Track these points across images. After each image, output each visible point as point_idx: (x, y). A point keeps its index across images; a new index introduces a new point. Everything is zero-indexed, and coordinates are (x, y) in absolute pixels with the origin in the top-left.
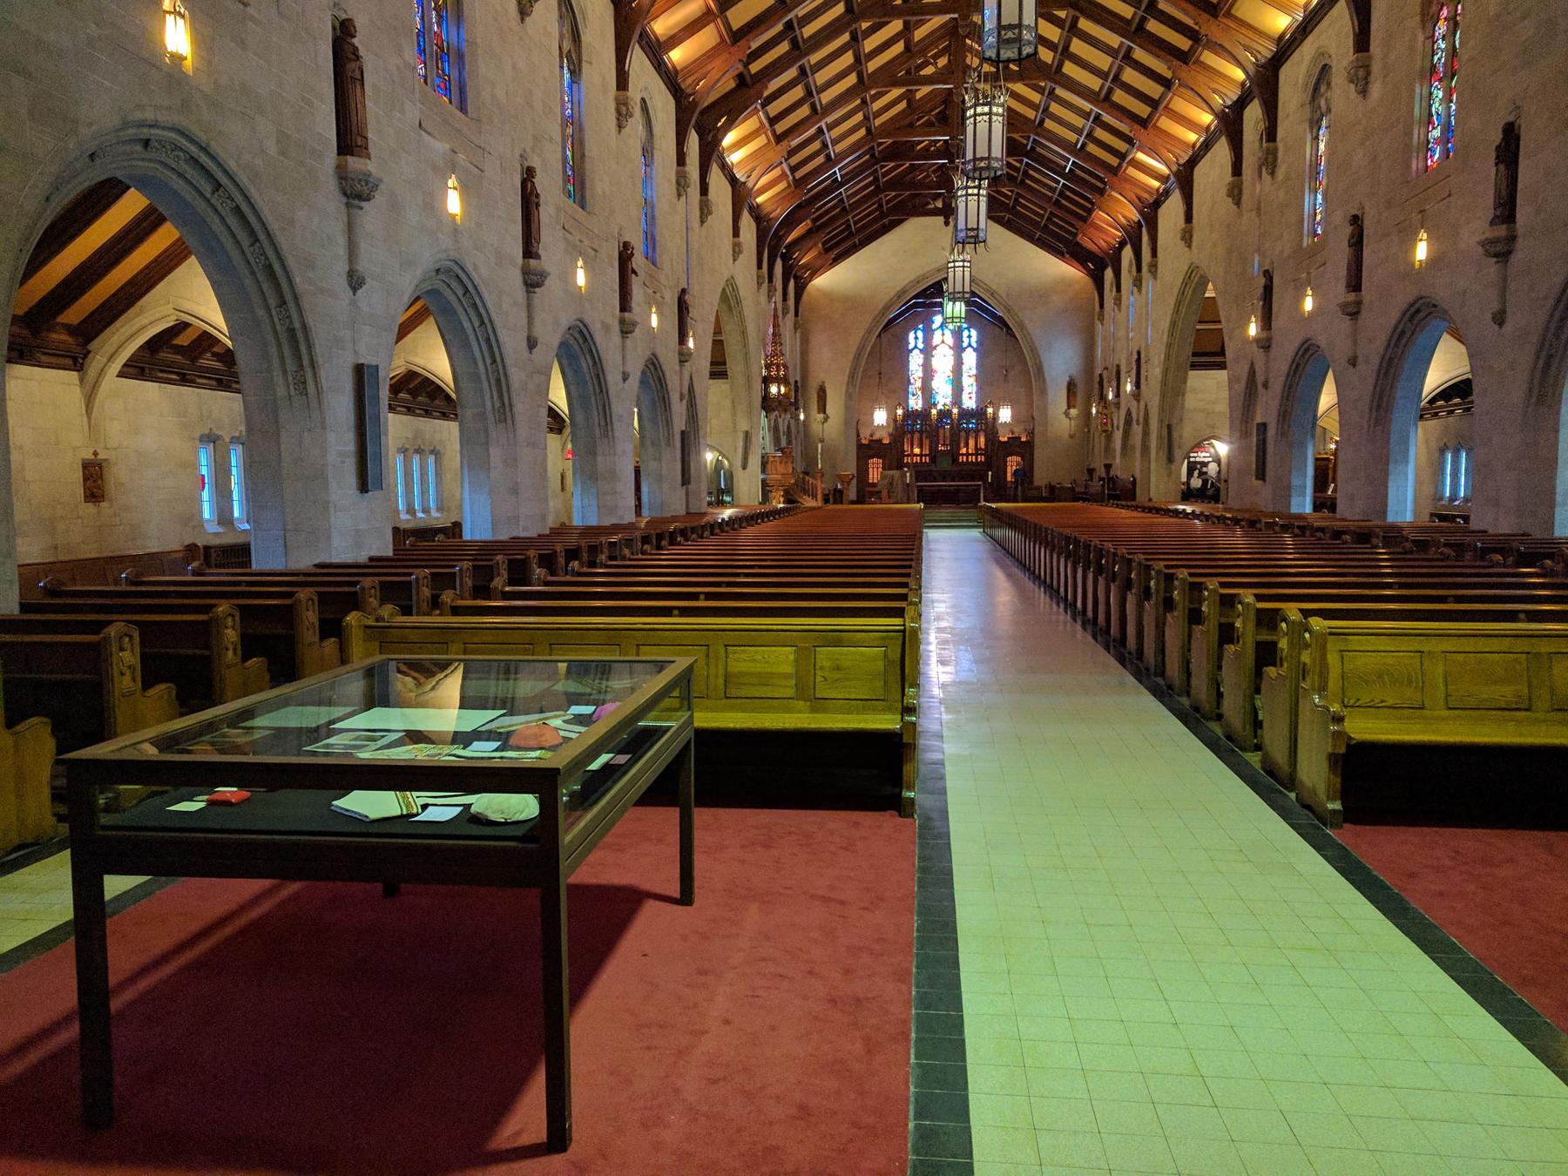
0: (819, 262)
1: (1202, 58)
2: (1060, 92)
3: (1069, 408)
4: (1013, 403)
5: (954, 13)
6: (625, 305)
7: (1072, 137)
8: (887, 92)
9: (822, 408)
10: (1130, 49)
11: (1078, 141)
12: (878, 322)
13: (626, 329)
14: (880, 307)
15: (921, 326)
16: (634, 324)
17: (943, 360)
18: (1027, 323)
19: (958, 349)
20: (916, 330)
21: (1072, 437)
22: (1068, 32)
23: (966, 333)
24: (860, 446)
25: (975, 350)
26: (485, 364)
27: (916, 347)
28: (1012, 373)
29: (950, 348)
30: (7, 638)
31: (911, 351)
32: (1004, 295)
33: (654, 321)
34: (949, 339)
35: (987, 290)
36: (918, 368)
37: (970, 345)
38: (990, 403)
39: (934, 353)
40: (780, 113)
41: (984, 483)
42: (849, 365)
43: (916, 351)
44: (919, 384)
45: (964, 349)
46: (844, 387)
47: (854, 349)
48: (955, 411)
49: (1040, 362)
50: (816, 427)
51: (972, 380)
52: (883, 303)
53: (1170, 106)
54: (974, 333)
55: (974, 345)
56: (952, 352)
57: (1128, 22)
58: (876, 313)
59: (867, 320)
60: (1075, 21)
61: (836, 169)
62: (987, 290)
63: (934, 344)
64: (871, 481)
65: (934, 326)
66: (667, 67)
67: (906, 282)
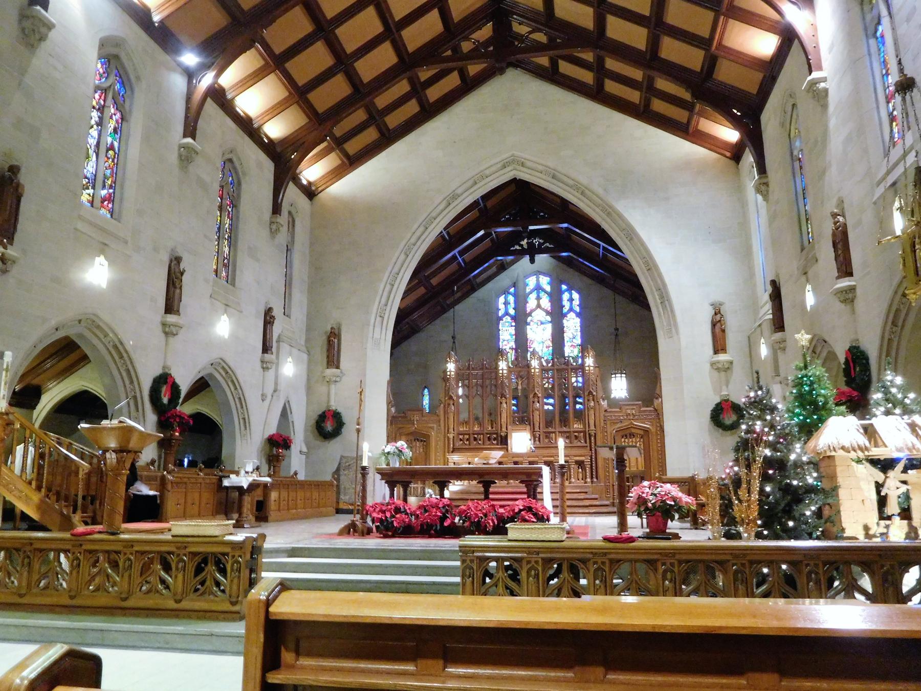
2: (611, 64)
5: (596, 494)
6: (171, 307)
19: (557, 315)
23: (566, 296)
25: (578, 315)
26: (222, 376)
29: (548, 313)
31: (501, 319)
34: (546, 302)
36: (509, 337)
37: (571, 309)
39: (529, 319)
45: (565, 315)
54: (576, 296)
55: (577, 309)
56: (549, 318)
60: (600, 61)
61: (456, 251)
63: (528, 310)
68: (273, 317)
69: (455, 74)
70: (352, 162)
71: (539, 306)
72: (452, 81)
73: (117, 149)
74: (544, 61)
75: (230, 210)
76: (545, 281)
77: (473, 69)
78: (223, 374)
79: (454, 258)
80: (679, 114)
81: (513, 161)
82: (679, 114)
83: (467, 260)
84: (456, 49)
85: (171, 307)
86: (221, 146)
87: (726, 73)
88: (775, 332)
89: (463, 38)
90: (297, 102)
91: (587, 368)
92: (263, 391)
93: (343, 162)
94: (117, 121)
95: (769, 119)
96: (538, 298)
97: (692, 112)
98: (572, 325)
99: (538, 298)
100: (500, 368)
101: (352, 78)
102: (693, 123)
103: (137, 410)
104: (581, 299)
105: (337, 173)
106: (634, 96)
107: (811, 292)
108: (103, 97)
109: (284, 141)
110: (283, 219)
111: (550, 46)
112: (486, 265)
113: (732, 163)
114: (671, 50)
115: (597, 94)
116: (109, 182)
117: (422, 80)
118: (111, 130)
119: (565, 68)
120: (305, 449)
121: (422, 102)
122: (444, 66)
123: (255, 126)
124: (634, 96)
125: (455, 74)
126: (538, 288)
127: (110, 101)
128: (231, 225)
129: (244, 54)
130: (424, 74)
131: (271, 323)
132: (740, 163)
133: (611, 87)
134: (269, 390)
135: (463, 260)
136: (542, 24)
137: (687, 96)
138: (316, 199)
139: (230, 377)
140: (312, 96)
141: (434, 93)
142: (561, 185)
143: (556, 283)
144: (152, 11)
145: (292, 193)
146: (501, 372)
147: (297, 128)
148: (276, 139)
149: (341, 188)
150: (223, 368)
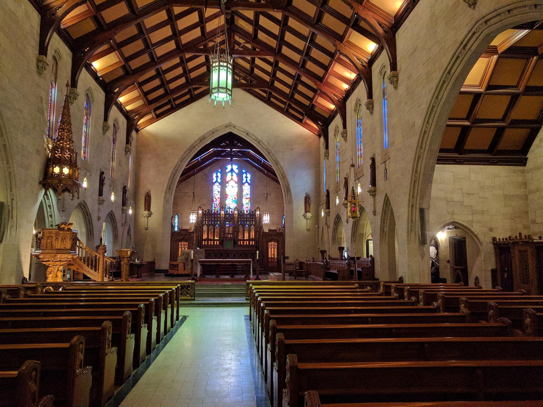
3: (306, 212)
4: (271, 214)
6: (101, 194)
7: (283, 106)
8: (199, 88)
9: (148, 207)
10: (299, 76)
11: (285, 107)
13: (101, 202)
14: (188, 146)
15: (220, 170)
16: (103, 201)
17: (232, 190)
18: (279, 160)
19: (240, 183)
23: (244, 175)
24: (173, 233)
25: (249, 184)
27: (217, 181)
28: (269, 198)
29: (236, 182)
30: (2, 311)
32: (266, 143)
33: (113, 198)
34: (235, 178)
35: (256, 140)
37: (247, 182)
39: (227, 185)
41: (253, 260)
42: (167, 180)
43: (217, 184)
44: (218, 202)
45: (244, 184)
46: (163, 194)
49: (289, 185)
50: (143, 220)
51: (248, 201)
52: (192, 142)
54: (249, 175)
55: (249, 181)
56: (236, 185)
57: (288, 95)
58: (185, 149)
59: (180, 153)
60: (277, 63)
61: (199, 157)
62: (256, 140)
63: (227, 180)
64: (270, 256)
65: (227, 171)
66: (118, 103)
67: (206, 132)
68: (126, 190)
69: (196, 13)
70: (159, 117)
71: (232, 179)
76: (235, 167)
79: (198, 159)
80: (301, 117)
82: (301, 117)
88: (327, 209)
89: (210, 40)
90: (142, 99)
93: (140, 95)
96: (232, 175)
97: (316, 94)
99: (232, 175)
104: (251, 178)
105: (151, 122)
109: (132, 111)
111: (252, 52)
113: (318, 137)
125: (196, 13)
126: (232, 171)
130: (188, 56)
136: (248, 74)
138: (139, 132)
140: (148, 96)
143: (239, 169)
145: (114, 110)
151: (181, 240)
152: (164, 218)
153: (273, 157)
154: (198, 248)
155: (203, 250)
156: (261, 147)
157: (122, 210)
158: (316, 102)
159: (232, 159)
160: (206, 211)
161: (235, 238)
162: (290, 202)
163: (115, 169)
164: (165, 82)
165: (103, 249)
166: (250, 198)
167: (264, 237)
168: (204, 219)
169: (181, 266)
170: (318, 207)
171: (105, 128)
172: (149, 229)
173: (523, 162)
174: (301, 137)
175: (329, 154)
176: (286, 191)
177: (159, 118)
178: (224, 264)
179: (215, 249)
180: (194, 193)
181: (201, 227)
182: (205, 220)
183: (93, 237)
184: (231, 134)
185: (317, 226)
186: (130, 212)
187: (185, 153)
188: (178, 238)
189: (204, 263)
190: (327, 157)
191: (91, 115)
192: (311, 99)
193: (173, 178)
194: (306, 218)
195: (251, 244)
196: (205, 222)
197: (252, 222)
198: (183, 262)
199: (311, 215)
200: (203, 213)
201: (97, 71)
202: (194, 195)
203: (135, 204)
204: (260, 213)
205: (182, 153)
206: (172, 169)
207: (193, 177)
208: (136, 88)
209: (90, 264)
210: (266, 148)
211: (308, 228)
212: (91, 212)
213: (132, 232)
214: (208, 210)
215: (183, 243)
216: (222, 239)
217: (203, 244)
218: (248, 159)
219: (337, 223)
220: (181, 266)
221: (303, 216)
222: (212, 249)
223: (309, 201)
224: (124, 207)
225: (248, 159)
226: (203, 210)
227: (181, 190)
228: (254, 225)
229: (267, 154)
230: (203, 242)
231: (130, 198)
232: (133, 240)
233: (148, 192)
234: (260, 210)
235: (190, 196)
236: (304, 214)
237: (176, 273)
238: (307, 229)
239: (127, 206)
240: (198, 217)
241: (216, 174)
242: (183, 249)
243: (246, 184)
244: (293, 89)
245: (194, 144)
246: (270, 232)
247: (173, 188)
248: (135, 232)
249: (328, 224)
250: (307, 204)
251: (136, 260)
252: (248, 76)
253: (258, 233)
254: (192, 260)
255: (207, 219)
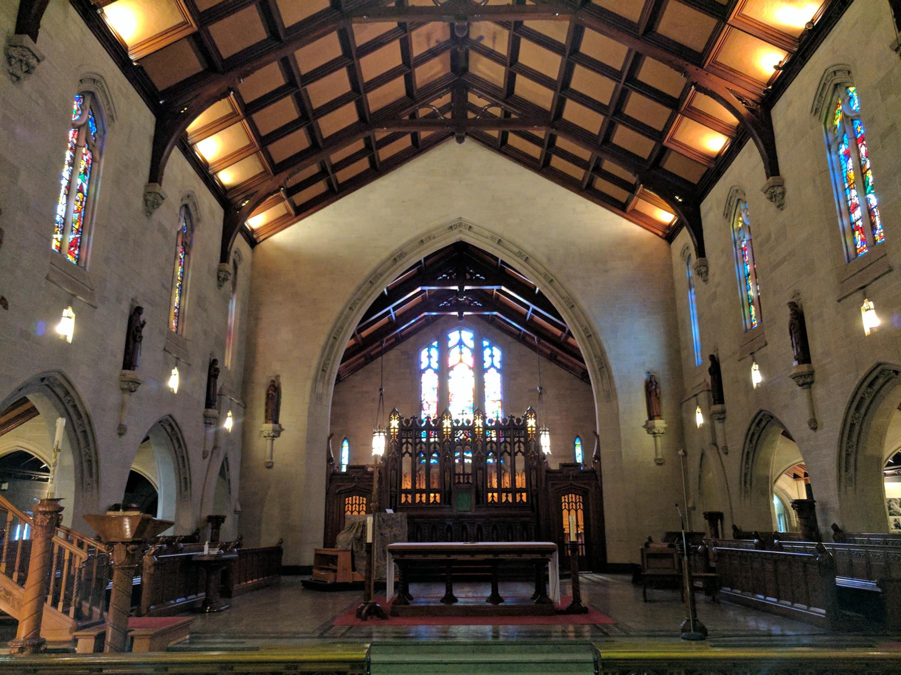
0: (263, 189)
1: (637, 208)
2: (562, 142)
3: (651, 417)
6: (129, 362)
9: (273, 414)
12: (365, 293)
14: (367, 272)
15: (435, 344)
19: (479, 370)
20: (430, 346)
21: (659, 463)
22: (547, 149)
23: (487, 352)
24: (333, 476)
25: (498, 371)
27: (429, 367)
29: (470, 368)
31: (423, 371)
32: (544, 260)
34: (469, 359)
35: (520, 254)
38: (531, 411)
40: (304, 181)
42: (318, 352)
45: (486, 371)
46: (309, 384)
47: (327, 328)
48: (479, 422)
49: (603, 353)
50: (261, 445)
52: (374, 265)
53: (693, 105)
54: (497, 352)
55: (498, 366)
56: (471, 373)
58: (359, 281)
59: (348, 290)
60: (552, 139)
61: (390, 308)
62: (520, 254)
63: (450, 365)
65: (450, 344)
66: (198, 159)
67: (404, 240)
68: (217, 370)
70: (301, 211)
72: (405, 142)
73: (85, 191)
74: (495, 133)
75: (182, 257)
77: (424, 134)
78: (169, 430)
79: (389, 312)
81: (460, 225)
82: (620, 194)
83: (397, 315)
84: (413, 116)
85: (129, 362)
86: (180, 191)
87: (671, 164)
89: (423, 104)
91: (529, 429)
92: (204, 447)
93: (252, 143)
94: (87, 161)
95: (711, 208)
97: (633, 193)
98: (494, 382)
100: (445, 426)
101: (313, 133)
102: (632, 203)
103: (91, 475)
105: (282, 223)
106: (578, 173)
107: (758, 372)
108: (76, 136)
109: (234, 189)
110: (229, 267)
112: (413, 321)
113: (664, 242)
114: (623, 137)
115: (542, 167)
116: (77, 226)
117: (378, 139)
118: (81, 170)
119: (514, 140)
120: (239, 509)
121: (372, 162)
122: (396, 130)
123: (210, 172)
124: (578, 173)
126: (461, 343)
127: (82, 142)
128: (183, 273)
129: (219, 102)
130: (381, 134)
131: (216, 376)
132: (673, 244)
133: (557, 162)
134: (209, 447)
135: (395, 314)
137: (631, 178)
138: (258, 247)
139: (176, 434)
140: (273, 148)
141: (385, 153)
142: (507, 251)
143: (478, 340)
144: (129, 49)
146: (445, 430)
147: (251, 176)
148: (228, 186)
149: (284, 237)
150: (170, 425)
151: (350, 493)
152: (311, 440)
153: (561, 290)
154: (390, 511)
155: (401, 516)
156: (531, 269)
157: (206, 417)
158: (672, 139)
159: (461, 314)
160: (407, 421)
161: (480, 484)
162: (610, 395)
163: (186, 314)
164: (298, 79)
165: (45, 513)
166: (500, 400)
167: (550, 483)
168: (404, 441)
169: (344, 560)
170: (681, 404)
171: (152, 202)
172: (274, 467)
173: (724, 422)
174: (624, 243)
175: (707, 268)
176: (597, 368)
177: (303, 215)
178: (468, 557)
179: (431, 513)
180: (381, 389)
181: (396, 461)
182: (407, 442)
183: (97, 482)
184: (461, 247)
185: (681, 452)
186: (229, 424)
187: (359, 288)
188: (342, 488)
189: (407, 557)
190: (704, 275)
191: (104, 151)
192: (657, 136)
193: (332, 346)
194: (654, 433)
195: (503, 501)
196: (407, 448)
197: (517, 445)
198: (350, 548)
199: (665, 425)
200: (402, 428)
201: (126, 47)
202: (381, 394)
203: (245, 408)
204: (536, 423)
205: (352, 289)
206: (329, 327)
207: (380, 358)
208: (237, 118)
209: (16, 568)
210: (542, 270)
211: (660, 457)
212: (89, 409)
213: (234, 473)
214: (414, 418)
215: (356, 499)
216: (447, 489)
217: (403, 500)
218: (495, 313)
219: (756, 437)
220: (344, 560)
221: (644, 427)
222: (424, 513)
223: (658, 391)
224: (210, 410)
225: (495, 313)
226: (400, 419)
227: (354, 387)
228: (523, 454)
229: (547, 284)
230: (403, 495)
231: (230, 391)
232: (235, 494)
233: (273, 378)
234: (535, 418)
235: (374, 400)
236: (647, 422)
237: (330, 578)
238: (656, 460)
239: (219, 409)
240: (388, 438)
241: (429, 351)
242: (355, 513)
243: (492, 369)
244: (626, 80)
245: (378, 268)
246: (565, 470)
247: (331, 370)
248: (242, 476)
249: (720, 442)
250: (653, 398)
251: (206, 547)
252: (501, 103)
253: (534, 473)
254: (370, 546)
255: (410, 440)
